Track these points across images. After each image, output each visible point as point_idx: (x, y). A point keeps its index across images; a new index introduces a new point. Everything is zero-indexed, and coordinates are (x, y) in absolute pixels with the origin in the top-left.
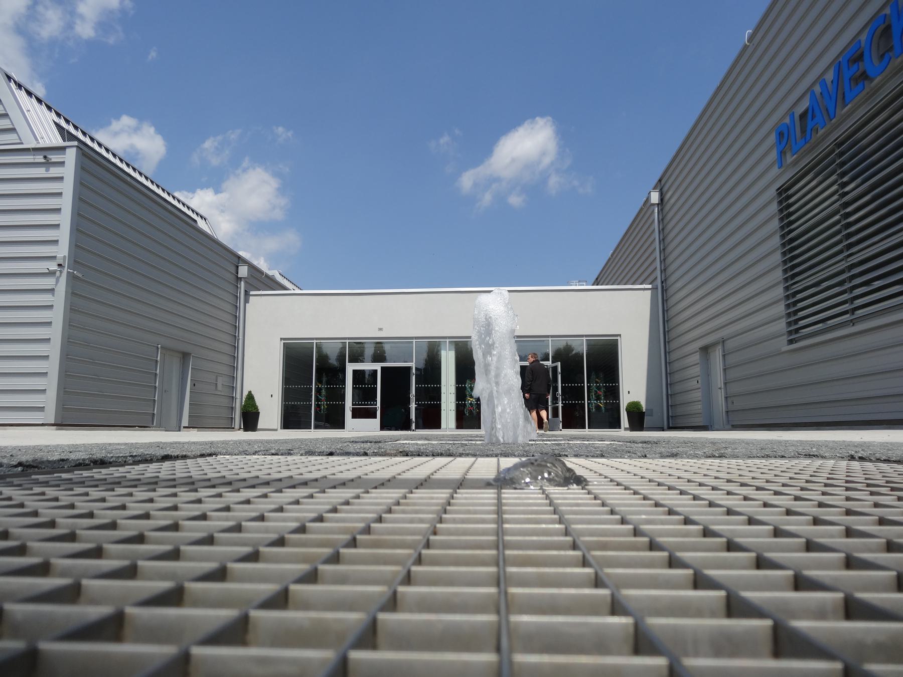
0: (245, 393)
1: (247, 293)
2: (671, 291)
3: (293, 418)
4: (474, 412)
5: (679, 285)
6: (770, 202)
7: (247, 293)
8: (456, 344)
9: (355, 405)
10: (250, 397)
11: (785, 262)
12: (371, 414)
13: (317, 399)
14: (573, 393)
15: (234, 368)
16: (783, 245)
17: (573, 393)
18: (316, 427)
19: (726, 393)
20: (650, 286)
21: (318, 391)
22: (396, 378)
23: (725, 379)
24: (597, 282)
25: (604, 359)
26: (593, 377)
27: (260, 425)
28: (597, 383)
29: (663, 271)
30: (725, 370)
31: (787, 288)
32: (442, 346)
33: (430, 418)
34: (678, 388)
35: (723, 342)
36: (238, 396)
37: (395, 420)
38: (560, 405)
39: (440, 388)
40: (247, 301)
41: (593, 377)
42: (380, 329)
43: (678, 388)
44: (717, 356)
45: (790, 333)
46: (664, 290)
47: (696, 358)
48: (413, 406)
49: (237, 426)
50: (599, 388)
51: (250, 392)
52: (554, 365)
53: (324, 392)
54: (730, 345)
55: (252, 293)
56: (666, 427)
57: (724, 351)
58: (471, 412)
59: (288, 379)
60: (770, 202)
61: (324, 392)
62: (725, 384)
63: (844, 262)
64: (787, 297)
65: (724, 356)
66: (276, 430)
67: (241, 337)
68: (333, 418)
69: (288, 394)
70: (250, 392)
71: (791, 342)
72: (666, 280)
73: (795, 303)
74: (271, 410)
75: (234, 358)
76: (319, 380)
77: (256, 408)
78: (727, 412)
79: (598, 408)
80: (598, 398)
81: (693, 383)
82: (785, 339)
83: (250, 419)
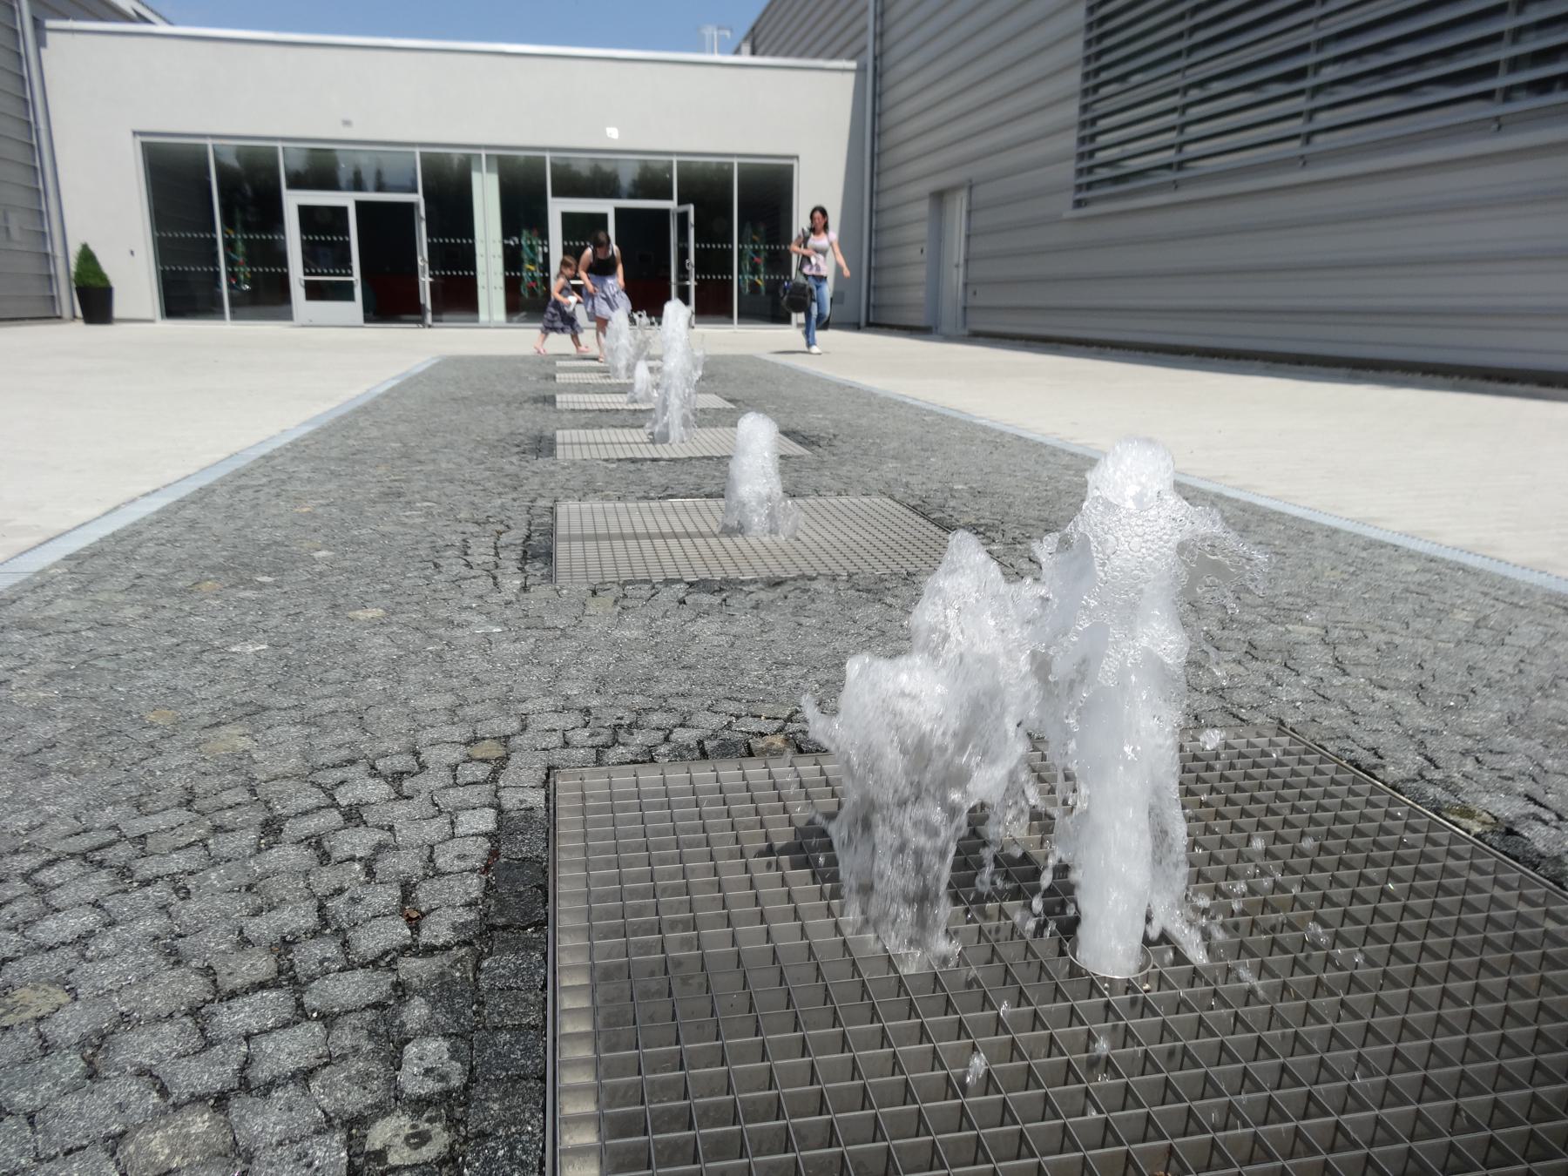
0: (74, 250)
1: (38, 24)
2: (890, 77)
3: (184, 296)
4: (539, 292)
5: (907, 66)
6: (1066, 99)
7: (38, 24)
8: (500, 159)
9: (311, 274)
10: (87, 256)
11: (1088, 60)
12: (342, 292)
13: (230, 262)
14: (713, 263)
15: (38, 193)
16: (1090, 27)
17: (713, 263)
18: (234, 317)
19: (966, 276)
20: (853, 65)
21: (229, 244)
22: (386, 226)
23: (967, 252)
24: (757, 40)
25: (767, 193)
26: (748, 230)
27: (118, 311)
28: (754, 242)
29: (880, 36)
30: (968, 237)
31: (1085, 108)
32: (474, 165)
33: (458, 297)
34: (888, 258)
35: (971, 188)
36: (59, 253)
37: (390, 302)
38: (692, 283)
39: (472, 248)
40: (41, 42)
41: (748, 230)
42: (347, 123)
43: (887, 238)
44: (958, 207)
45: (1079, 188)
46: (878, 75)
47: (923, 208)
48: (425, 280)
49: (67, 313)
50: (756, 252)
51: (85, 248)
52: (683, 208)
53: (240, 247)
54: (981, 194)
55: (50, 24)
56: (863, 322)
57: (970, 203)
58: (532, 292)
59: (162, 214)
60: (1066, 99)
61: (240, 247)
62: (967, 261)
63: (1178, 76)
64: (1083, 125)
65: (969, 212)
66: (151, 321)
67: (42, 126)
68: (266, 295)
69: (165, 251)
70: (85, 248)
71: (1079, 204)
72: (881, 55)
73: (1097, 72)
74: (134, 275)
75: (35, 171)
76: (228, 222)
77: (103, 278)
78: (965, 308)
79: (754, 286)
80: (755, 271)
81: (913, 253)
82: (1071, 196)
83: (96, 302)
